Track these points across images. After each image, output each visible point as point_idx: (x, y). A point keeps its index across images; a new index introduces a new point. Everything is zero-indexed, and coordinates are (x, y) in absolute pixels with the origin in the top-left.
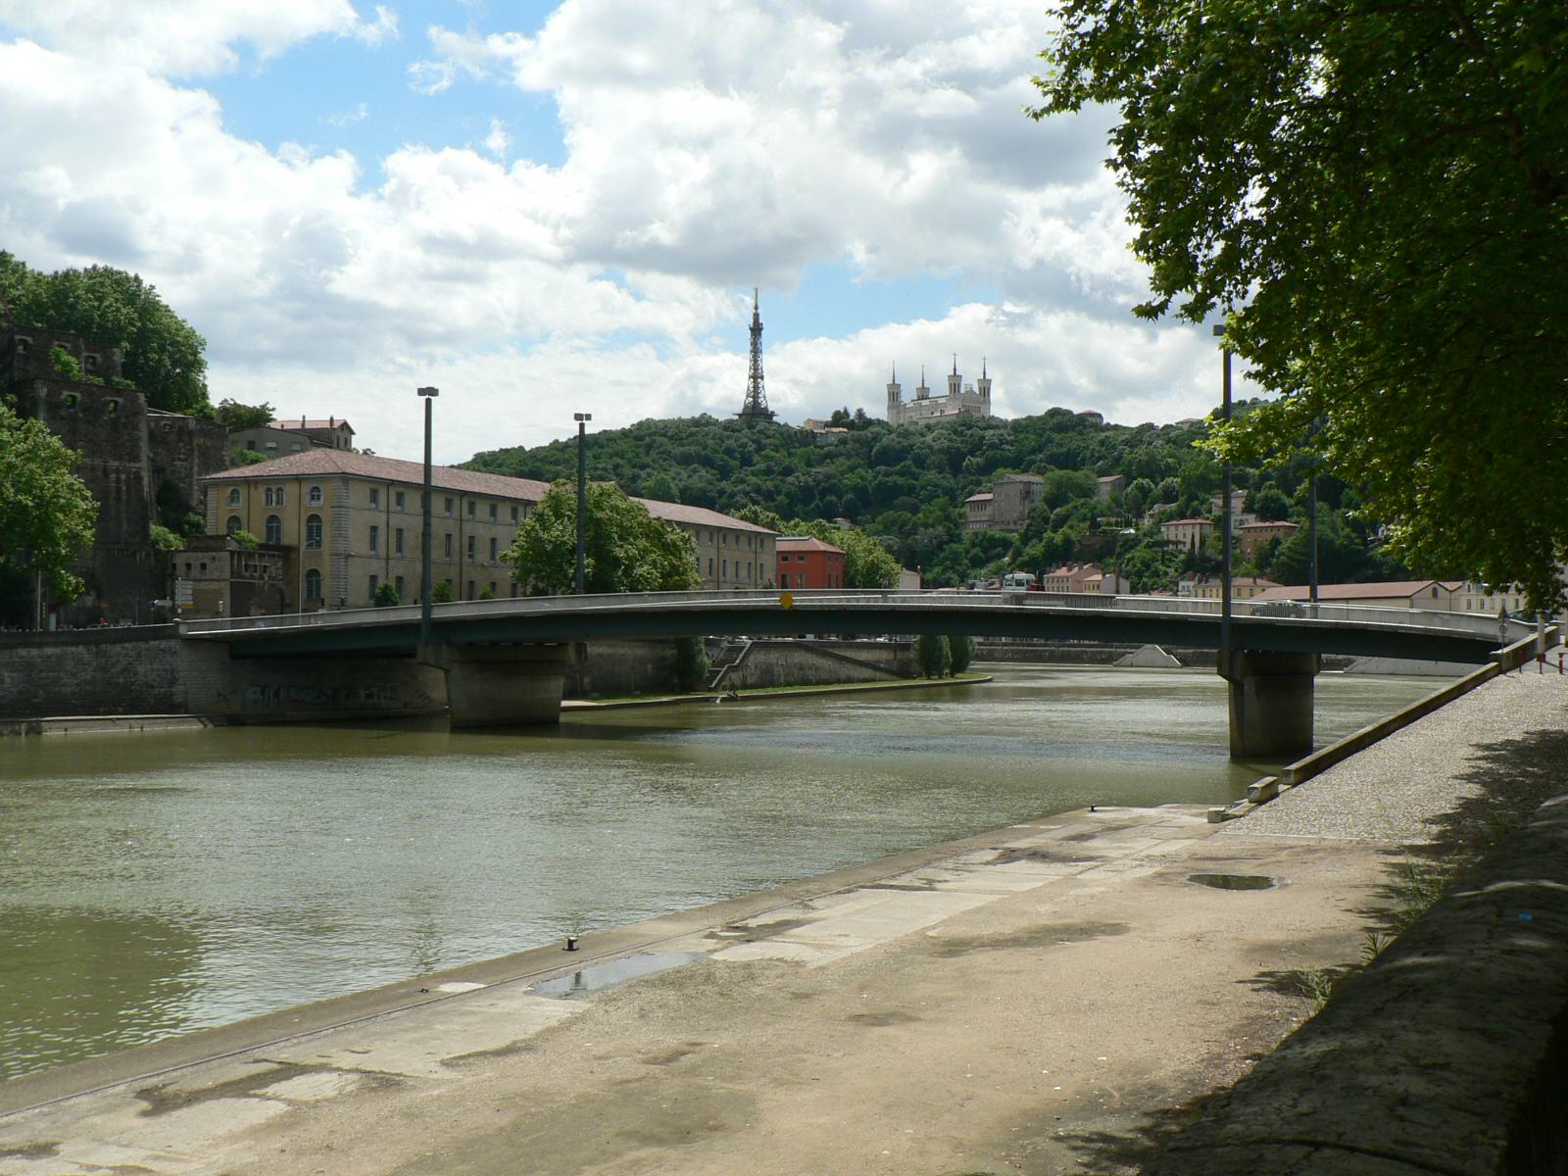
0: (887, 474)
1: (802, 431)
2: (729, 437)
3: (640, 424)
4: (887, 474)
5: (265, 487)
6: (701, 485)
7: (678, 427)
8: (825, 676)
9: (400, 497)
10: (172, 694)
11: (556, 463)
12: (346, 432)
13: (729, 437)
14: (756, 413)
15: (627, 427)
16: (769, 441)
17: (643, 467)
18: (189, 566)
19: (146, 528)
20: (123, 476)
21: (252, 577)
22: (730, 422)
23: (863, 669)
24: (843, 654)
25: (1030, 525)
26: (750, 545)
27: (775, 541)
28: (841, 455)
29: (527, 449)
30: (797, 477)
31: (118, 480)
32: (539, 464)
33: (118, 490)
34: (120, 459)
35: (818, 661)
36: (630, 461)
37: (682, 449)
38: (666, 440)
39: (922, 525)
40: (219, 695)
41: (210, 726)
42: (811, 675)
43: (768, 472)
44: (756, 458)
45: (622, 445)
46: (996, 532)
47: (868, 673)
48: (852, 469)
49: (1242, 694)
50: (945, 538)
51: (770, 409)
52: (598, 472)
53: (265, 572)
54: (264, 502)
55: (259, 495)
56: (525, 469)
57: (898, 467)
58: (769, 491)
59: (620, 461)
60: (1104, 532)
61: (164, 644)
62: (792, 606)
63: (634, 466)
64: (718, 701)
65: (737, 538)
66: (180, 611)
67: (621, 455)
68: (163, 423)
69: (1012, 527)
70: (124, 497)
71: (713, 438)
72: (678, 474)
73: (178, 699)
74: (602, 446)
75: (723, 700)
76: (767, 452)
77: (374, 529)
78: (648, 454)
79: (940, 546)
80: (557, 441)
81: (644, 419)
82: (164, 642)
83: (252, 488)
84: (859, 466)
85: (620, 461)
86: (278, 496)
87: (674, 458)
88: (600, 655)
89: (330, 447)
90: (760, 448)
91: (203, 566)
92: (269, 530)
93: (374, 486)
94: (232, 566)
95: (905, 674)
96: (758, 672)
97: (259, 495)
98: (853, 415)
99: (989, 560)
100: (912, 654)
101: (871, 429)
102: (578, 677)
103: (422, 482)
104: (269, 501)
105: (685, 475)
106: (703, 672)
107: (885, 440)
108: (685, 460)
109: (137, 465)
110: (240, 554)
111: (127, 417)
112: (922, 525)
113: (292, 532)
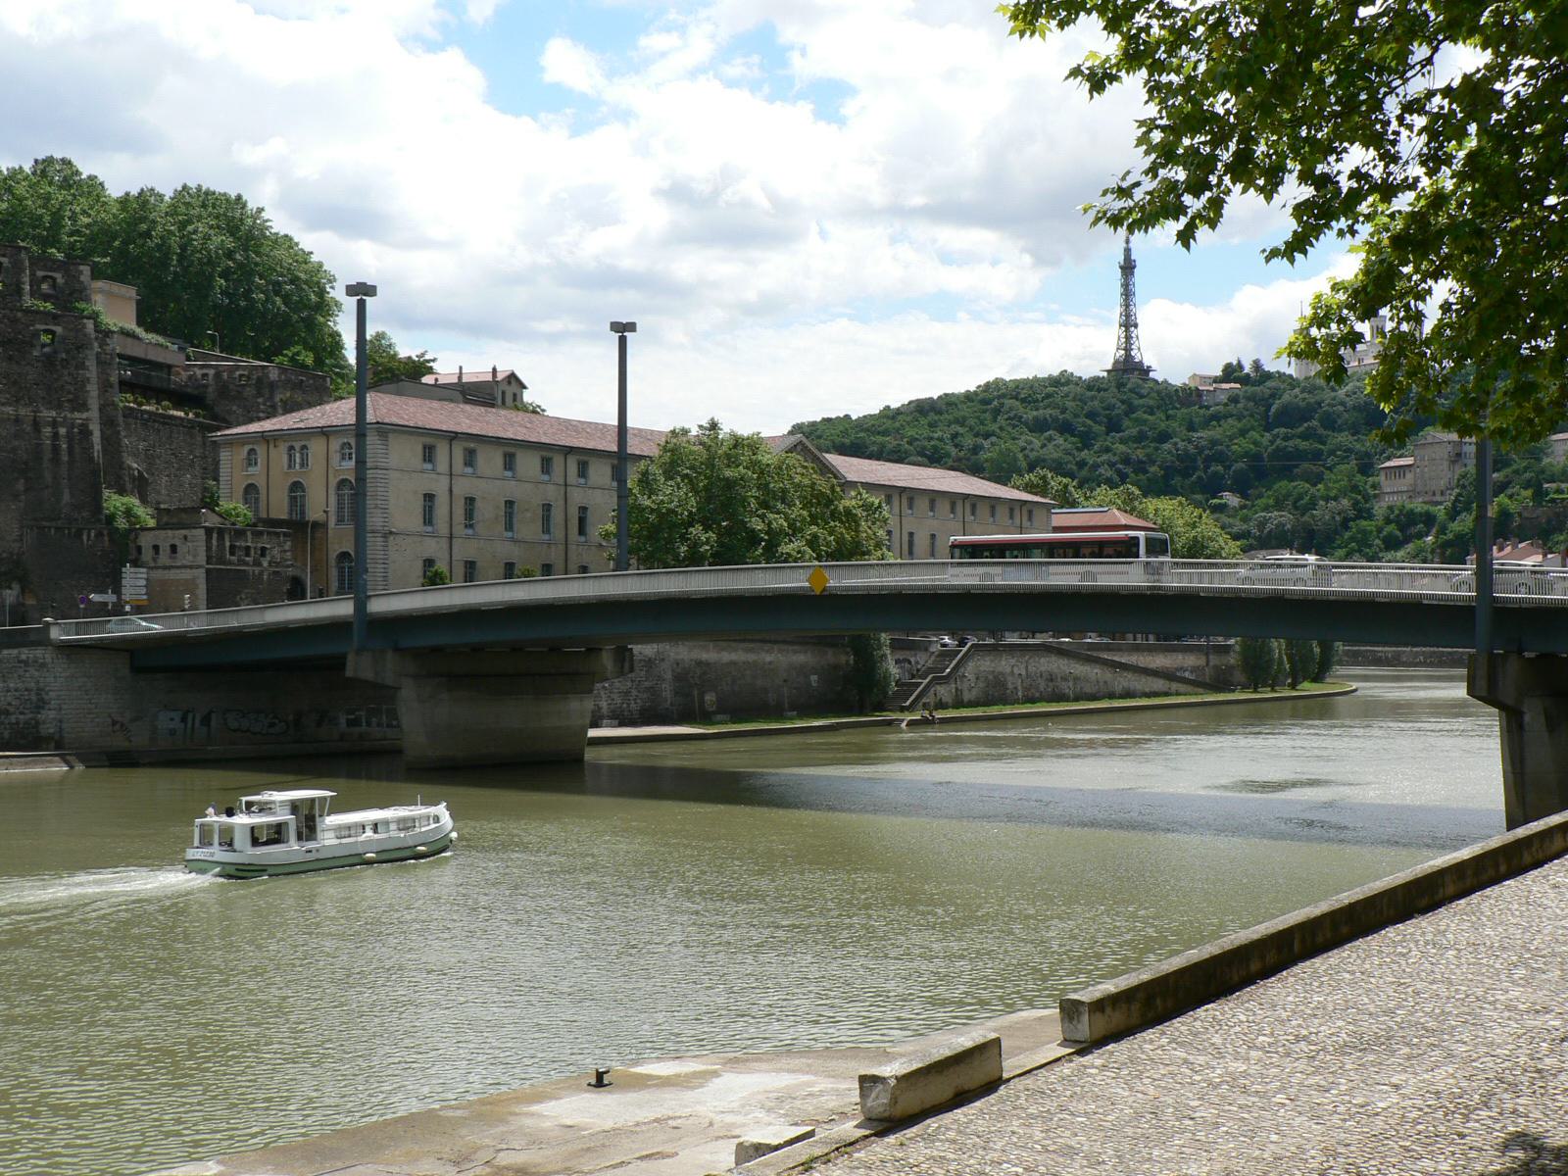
0: (1286, 438)
1: (1185, 389)
2: (1093, 398)
3: (988, 385)
4: (1286, 438)
5: (287, 444)
6: (1055, 455)
7: (1031, 387)
8: (1088, 689)
9: (470, 458)
10: (37, 723)
11: (885, 433)
12: (514, 388)
13: (1093, 398)
14: (1128, 369)
15: (972, 389)
16: (1141, 401)
17: (987, 436)
18: (156, 548)
19: (99, 494)
20: (62, 431)
21: (242, 562)
22: (1096, 379)
23: (1150, 679)
24: (1116, 659)
25: (1460, 495)
26: (1011, 517)
27: (1049, 511)
28: (1232, 416)
29: (854, 417)
30: (1176, 444)
31: (56, 436)
32: (862, 435)
33: (56, 449)
34: (59, 407)
35: (1079, 669)
36: (971, 429)
37: (1035, 413)
38: (1018, 403)
39: (1322, 498)
40: (114, 723)
41: (80, 768)
42: (1067, 688)
43: (1140, 438)
44: (1126, 423)
45: (965, 411)
46: (1418, 505)
47: (1159, 684)
48: (1243, 433)
49: (1521, 727)
50: (1352, 513)
51: (1146, 363)
52: (932, 443)
53: (263, 555)
54: (286, 466)
55: (280, 455)
56: (847, 441)
57: (1301, 429)
58: (1141, 462)
59: (961, 430)
60: (1553, 501)
61: (25, 653)
62: (824, 590)
63: (977, 435)
64: (904, 725)
65: (993, 508)
66: (128, 608)
67: (961, 422)
68: (238, 373)
69: (1438, 498)
70: (65, 458)
71: (1074, 400)
72: (1031, 442)
73: (49, 729)
74: (940, 413)
75: (911, 723)
76: (1139, 414)
77: (429, 498)
78: (995, 420)
79: (1345, 524)
80: (887, 408)
81: (991, 379)
82: (25, 650)
83: (271, 446)
84: (1253, 428)
85: (961, 430)
86: (302, 454)
87: (1026, 424)
88: (733, 663)
89: (493, 406)
90: (1131, 409)
91: (174, 549)
92: (293, 500)
93: (429, 440)
94: (209, 548)
95: (1221, 683)
96: (981, 685)
97: (280, 455)
98: (1247, 369)
99: (1407, 540)
100: (1232, 659)
101: (1269, 384)
102: (696, 692)
103: (615, 448)
104: (291, 464)
105: (1037, 443)
106: (889, 684)
107: (1286, 398)
108: (1039, 427)
109: (85, 415)
110: (221, 532)
111: (68, 352)
112: (1322, 498)
113: (320, 504)
